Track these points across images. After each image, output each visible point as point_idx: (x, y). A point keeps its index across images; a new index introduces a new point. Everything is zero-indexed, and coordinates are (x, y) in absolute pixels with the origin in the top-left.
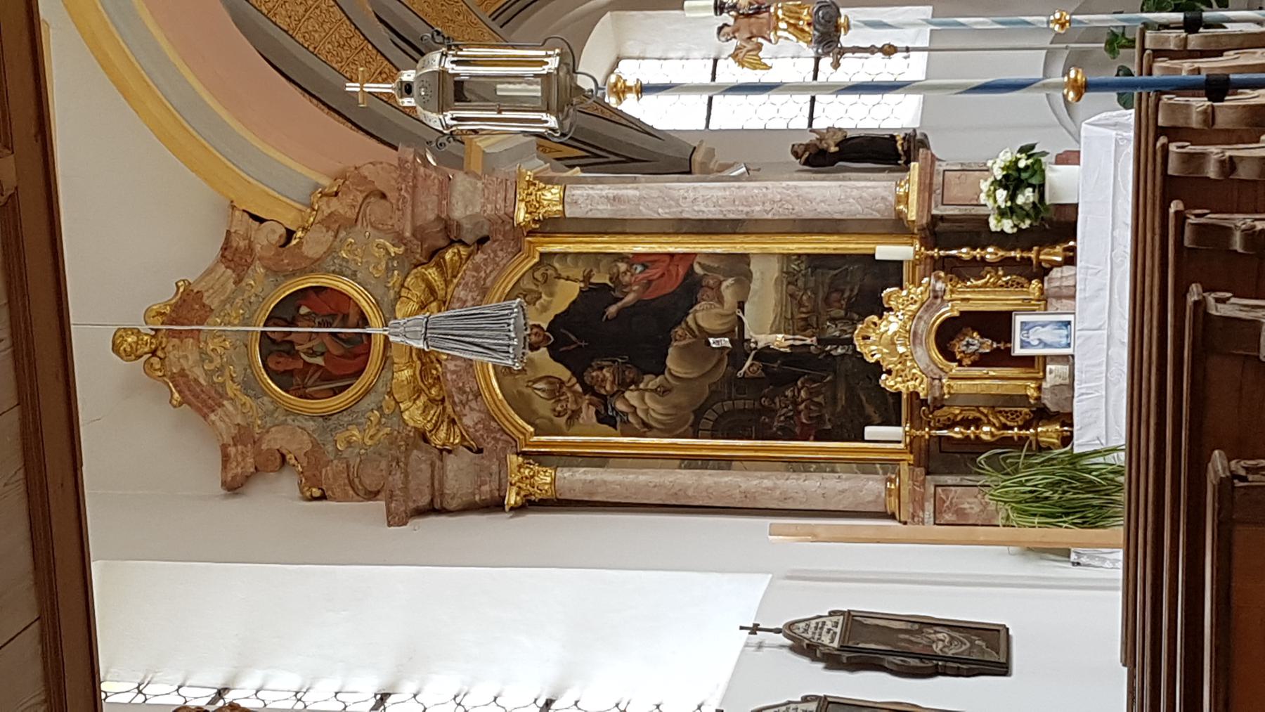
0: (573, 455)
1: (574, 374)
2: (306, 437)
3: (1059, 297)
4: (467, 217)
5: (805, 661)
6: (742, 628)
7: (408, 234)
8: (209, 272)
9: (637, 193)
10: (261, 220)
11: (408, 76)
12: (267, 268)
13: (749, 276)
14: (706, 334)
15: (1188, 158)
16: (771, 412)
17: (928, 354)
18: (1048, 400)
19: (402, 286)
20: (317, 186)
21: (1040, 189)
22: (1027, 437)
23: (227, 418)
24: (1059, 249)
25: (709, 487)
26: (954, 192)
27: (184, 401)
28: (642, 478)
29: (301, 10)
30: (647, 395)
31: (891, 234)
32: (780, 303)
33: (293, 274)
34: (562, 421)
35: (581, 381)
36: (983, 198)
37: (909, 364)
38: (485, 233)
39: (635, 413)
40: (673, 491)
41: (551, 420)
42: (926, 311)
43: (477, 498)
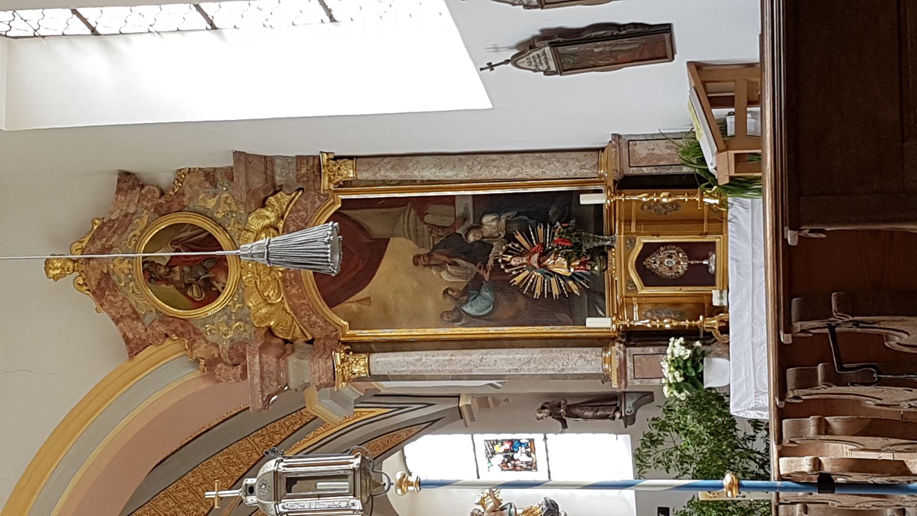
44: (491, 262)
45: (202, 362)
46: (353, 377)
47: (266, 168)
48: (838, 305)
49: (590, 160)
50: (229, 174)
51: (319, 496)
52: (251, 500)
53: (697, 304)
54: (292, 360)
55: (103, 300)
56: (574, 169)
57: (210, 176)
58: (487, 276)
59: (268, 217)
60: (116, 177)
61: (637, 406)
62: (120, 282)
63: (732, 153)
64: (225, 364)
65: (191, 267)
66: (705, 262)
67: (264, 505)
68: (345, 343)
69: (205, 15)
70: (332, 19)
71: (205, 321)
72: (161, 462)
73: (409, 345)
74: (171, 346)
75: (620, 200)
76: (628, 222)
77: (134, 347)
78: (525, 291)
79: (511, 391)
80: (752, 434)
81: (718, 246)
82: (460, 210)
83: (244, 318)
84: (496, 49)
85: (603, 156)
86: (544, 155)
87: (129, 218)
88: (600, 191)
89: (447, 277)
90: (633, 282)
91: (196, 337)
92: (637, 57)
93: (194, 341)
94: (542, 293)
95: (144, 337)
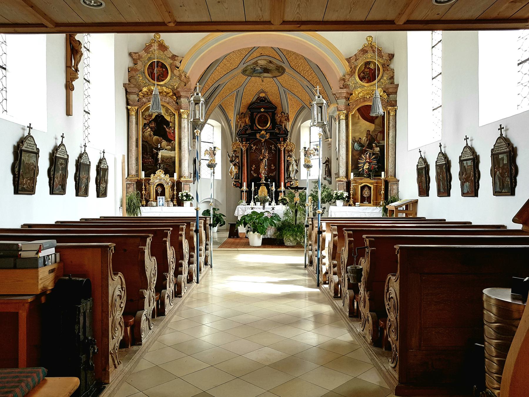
0: (138, 118)
1: (153, 119)
2: (140, 69)
3: (168, 204)
4: (181, 101)
5: (98, 161)
6: (104, 150)
7: (178, 90)
8: (171, 52)
9: (186, 131)
10: (180, 63)
11: (200, 94)
12: (172, 63)
13: (171, 151)
14: (161, 143)
15: (182, 229)
16: (147, 155)
17: (157, 182)
18: (150, 202)
19: (169, 88)
20: (187, 73)
21: (186, 200)
22: (143, 199)
23: (144, 54)
24: (176, 203)
25: (132, 143)
26: (186, 186)
27: (147, 46)
28: (134, 131)
29: (220, 71)
30: (150, 132)
31: (179, 175)
32: (167, 156)
33: (171, 68)
34: (144, 117)
35: (152, 120)
36: (184, 191)
37: (156, 179)
38: (179, 104)
39: (146, 130)
40: (131, 137)
41: (144, 115)
42: (165, 182)
43: (129, 101)
44: (367, 149)
45: (344, 77)
46: (340, 116)
47: (394, 92)
48: (373, 249)
49: (393, 174)
50: (392, 83)
51: (317, 114)
52: (317, 97)
53: (356, 199)
54: (344, 100)
55: (360, 51)
56: (390, 170)
57: (392, 78)
58: (364, 148)
59: (381, 93)
60: (393, 53)
61: (328, 180)
62: (365, 55)
63: (395, 209)
64: (344, 83)
65: (368, 74)
66: (366, 201)
67: (315, 101)
68: (348, 113)
69: (436, 77)
70: (433, 110)
71: (355, 78)
72: (318, 66)
73: (347, 129)
74: (348, 69)
75: (382, 181)
76: (377, 183)
77: (348, 60)
78: (360, 157)
79: (332, 151)
80: (322, 207)
81: (370, 204)
82: (381, 142)
83: (355, 88)
84: (425, 153)
85: (393, 177)
86: (394, 163)
87: (382, 57)
88: (385, 176)
89: (364, 139)
90: (362, 184)
91: (350, 75)
92: (420, 188)
93: (350, 75)
94: (359, 162)
95: (351, 62)
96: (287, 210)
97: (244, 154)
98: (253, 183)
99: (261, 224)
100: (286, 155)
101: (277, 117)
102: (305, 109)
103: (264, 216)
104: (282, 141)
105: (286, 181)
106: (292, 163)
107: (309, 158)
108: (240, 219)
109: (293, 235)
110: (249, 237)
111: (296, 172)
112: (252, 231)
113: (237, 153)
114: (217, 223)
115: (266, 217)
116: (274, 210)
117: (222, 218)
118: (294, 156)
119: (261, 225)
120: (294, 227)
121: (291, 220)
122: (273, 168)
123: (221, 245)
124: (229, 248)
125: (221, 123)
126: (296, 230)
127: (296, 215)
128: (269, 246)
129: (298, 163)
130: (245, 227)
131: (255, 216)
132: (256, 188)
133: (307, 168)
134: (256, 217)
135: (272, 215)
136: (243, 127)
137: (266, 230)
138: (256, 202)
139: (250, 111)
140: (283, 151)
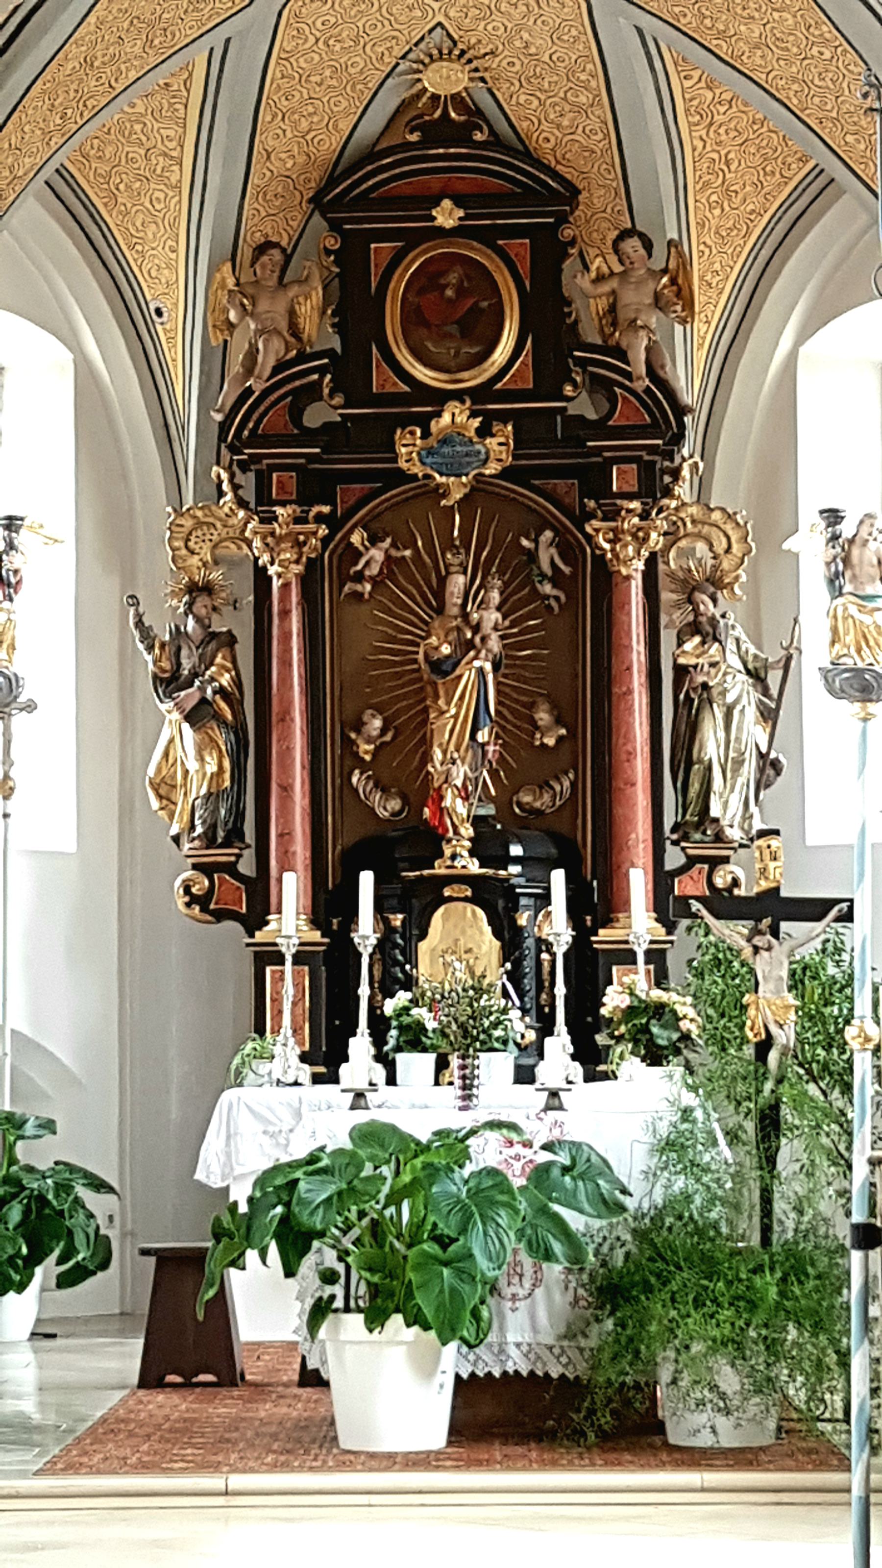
96: (686, 1113)
97: (285, 613)
98: (367, 880)
99: (443, 1242)
100: (664, 619)
101: (584, 282)
102: (844, 197)
103: (469, 1169)
104: (630, 497)
105: (674, 858)
106: (724, 693)
107: (871, 605)
108: (251, 1200)
109: (740, 1347)
110: (331, 1373)
111: (761, 770)
112: (359, 1310)
113: (215, 609)
114: (35, 1258)
115: (492, 1172)
116: (561, 1108)
117: (77, 1201)
118: (739, 632)
119: (444, 1247)
120: (754, 1271)
121: (724, 1202)
122: (550, 741)
123: (67, 1450)
124: (144, 1467)
125: (72, 342)
126: (773, 1293)
127: (769, 1161)
128: (520, 1450)
129: (774, 692)
130: (290, 1272)
131: (386, 1171)
132: (397, 920)
133: (852, 699)
134: (397, 1173)
135: (545, 1157)
136: (276, 370)
137: (489, 1300)
138: (398, 1049)
139: (335, 226)
140: (636, 587)
